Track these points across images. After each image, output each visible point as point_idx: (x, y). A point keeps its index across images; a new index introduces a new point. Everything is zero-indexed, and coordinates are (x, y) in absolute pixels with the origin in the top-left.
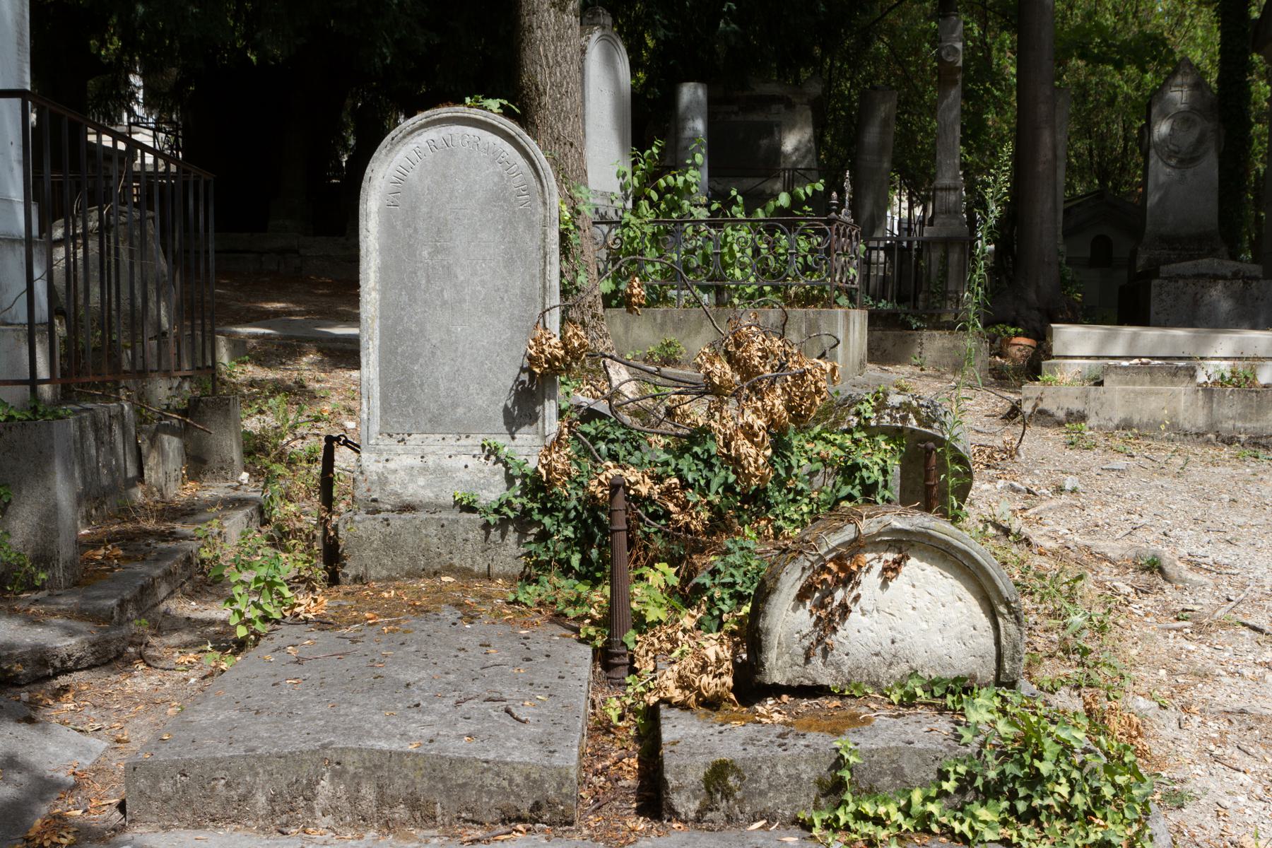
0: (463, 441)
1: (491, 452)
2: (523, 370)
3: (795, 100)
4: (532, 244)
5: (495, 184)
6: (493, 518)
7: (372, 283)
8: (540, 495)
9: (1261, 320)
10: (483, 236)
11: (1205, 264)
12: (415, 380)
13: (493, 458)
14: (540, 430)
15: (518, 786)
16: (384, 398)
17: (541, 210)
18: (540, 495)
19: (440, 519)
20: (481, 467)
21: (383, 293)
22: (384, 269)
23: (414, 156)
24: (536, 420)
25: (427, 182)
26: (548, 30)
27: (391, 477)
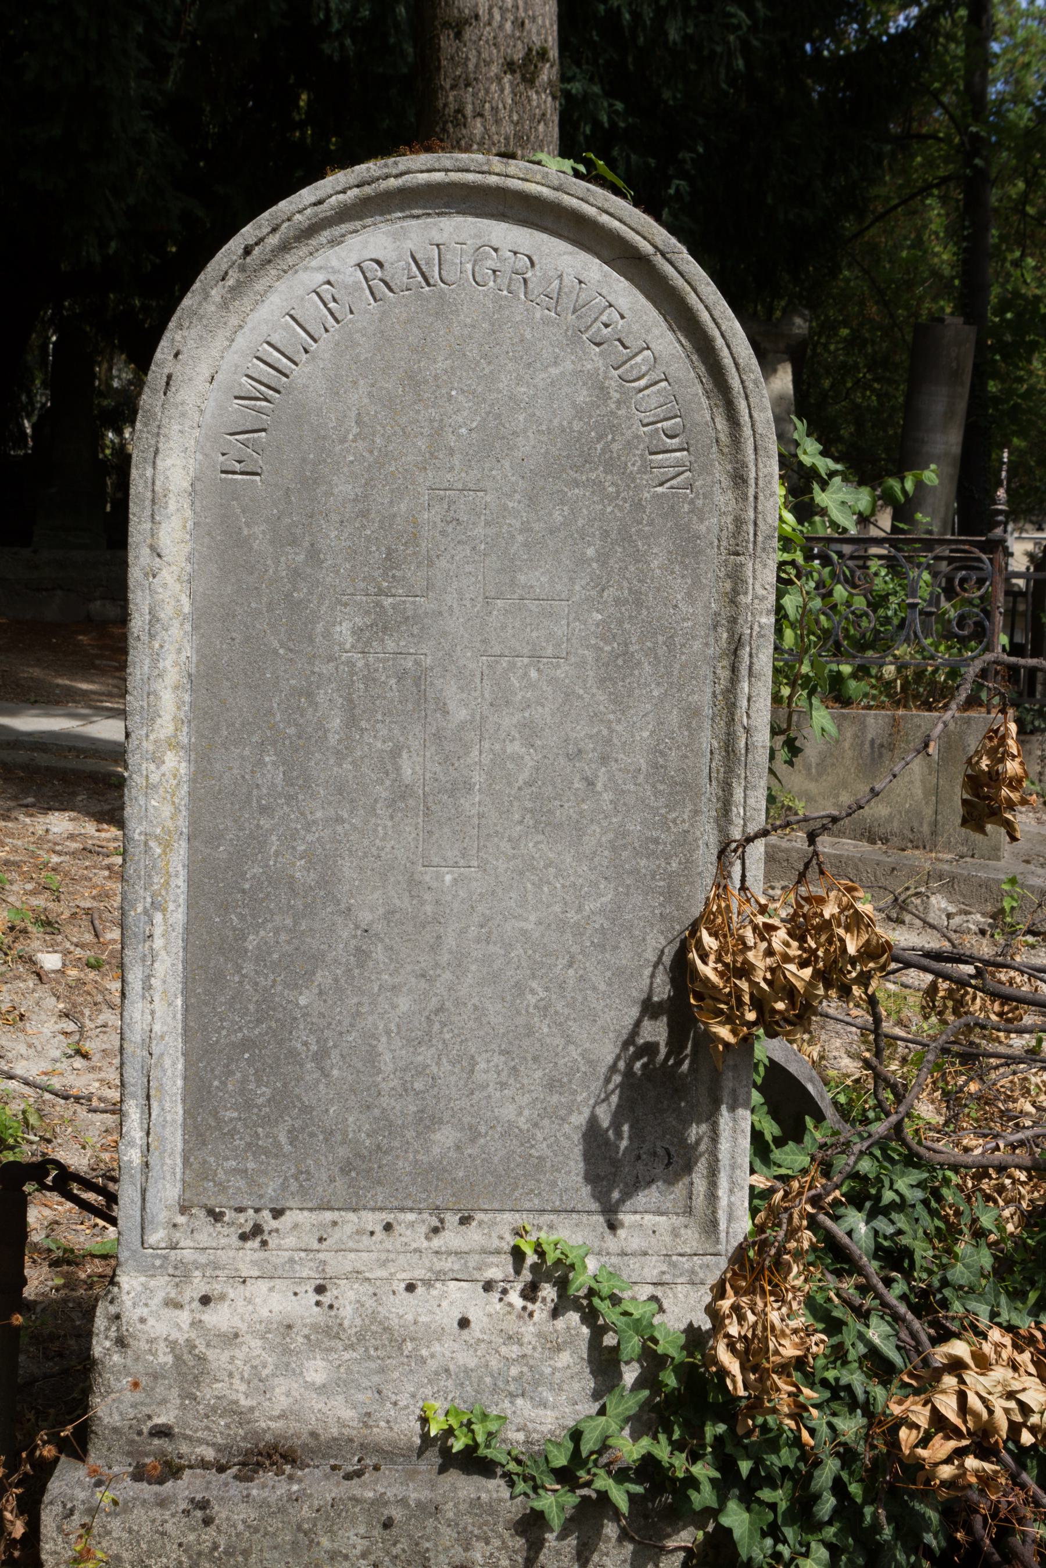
0: (452, 1238)
1: (547, 1275)
2: (649, 1009)
4: (693, 609)
5: (580, 413)
6: (555, 1502)
7: (165, 726)
8: (714, 1430)
9: (112, 611)
10: (535, 578)
12: (303, 1040)
13: (548, 1292)
14: (699, 1200)
16: (198, 1095)
17: (724, 499)
18: (714, 1430)
19: (380, 1501)
20: (511, 1325)
21: (202, 758)
22: (205, 679)
23: (313, 311)
24: (688, 1168)
25: (357, 397)
26: (498, 122)
27: (218, 1358)
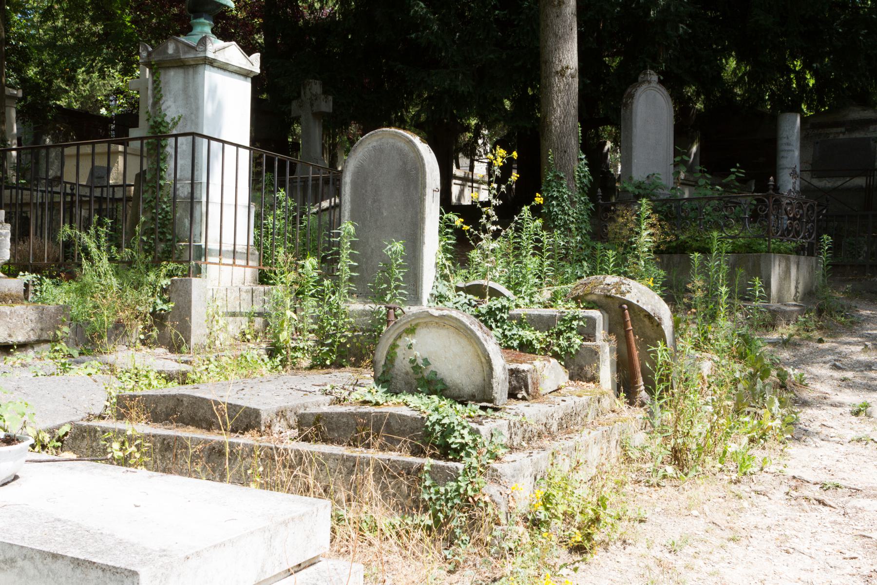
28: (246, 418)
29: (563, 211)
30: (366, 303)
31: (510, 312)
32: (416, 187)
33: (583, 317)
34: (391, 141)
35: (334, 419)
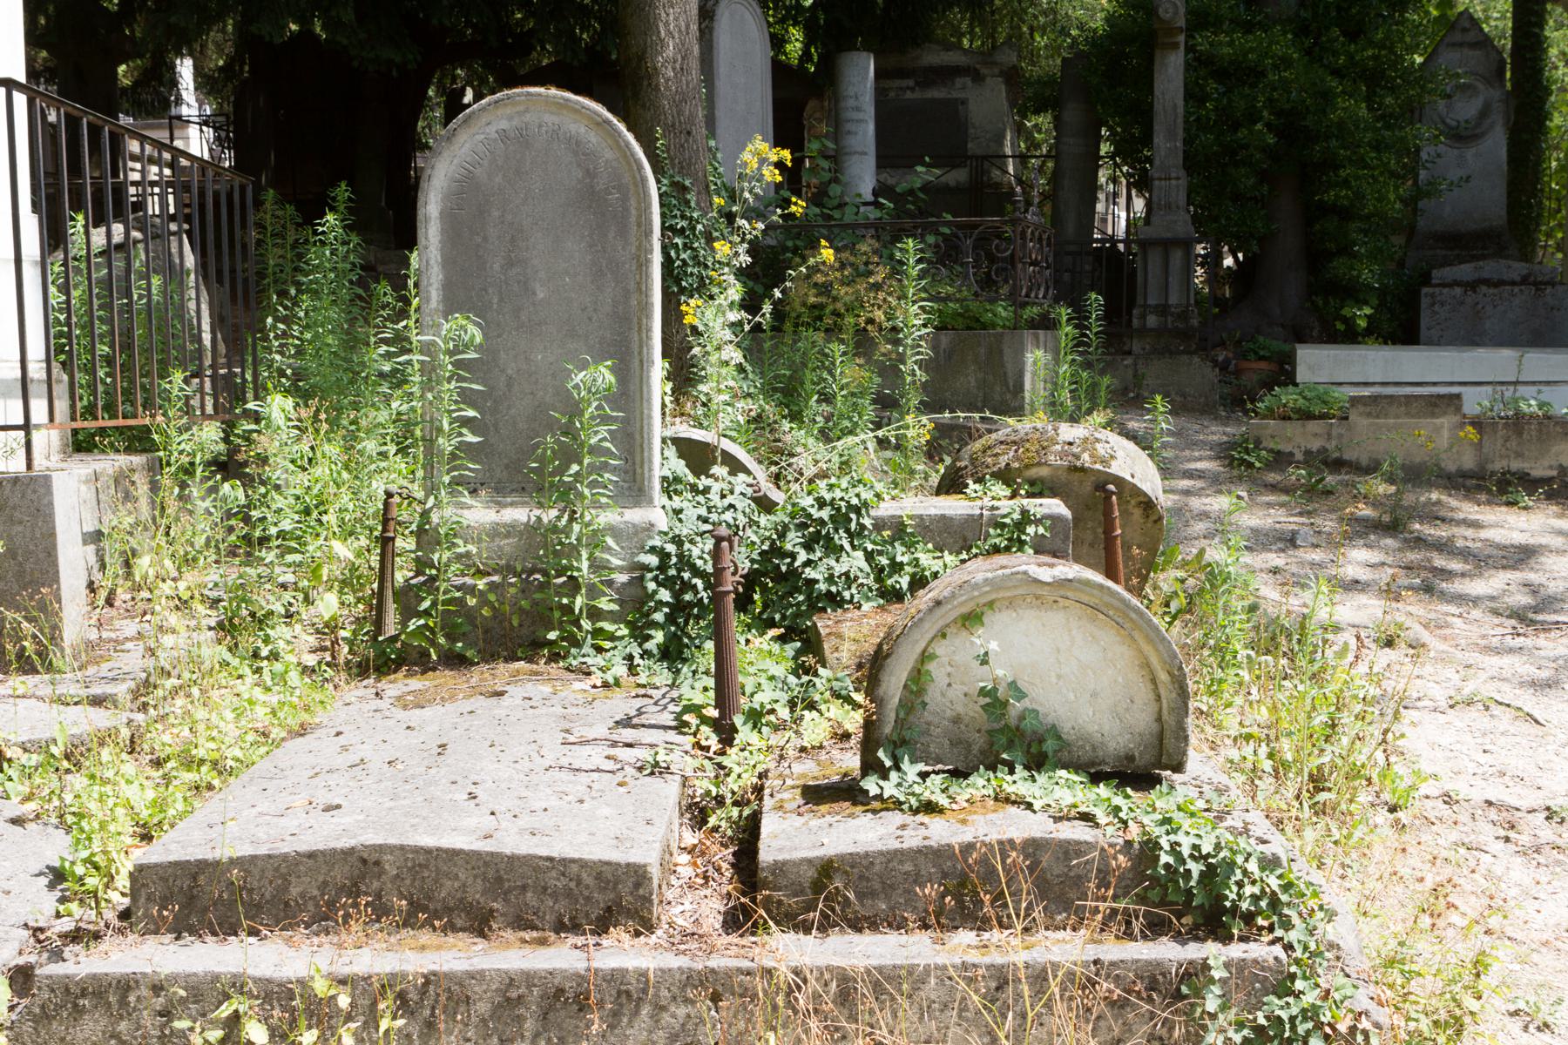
3: (984, 71)
11: (1489, 268)
15: (587, 887)
28: (603, 890)
29: (695, 258)
30: (501, 505)
31: (873, 513)
32: (623, 232)
33: (1046, 517)
34: (549, 119)
35: (877, 868)
